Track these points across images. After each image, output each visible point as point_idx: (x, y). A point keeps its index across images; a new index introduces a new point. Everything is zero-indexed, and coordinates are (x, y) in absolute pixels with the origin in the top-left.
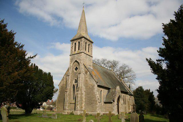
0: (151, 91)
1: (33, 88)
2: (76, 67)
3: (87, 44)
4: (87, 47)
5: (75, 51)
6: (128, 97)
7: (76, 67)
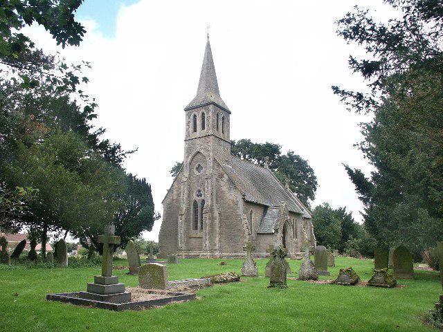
0: (176, 164)
1: (102, 204)
2: (199, 165)
3: (221, 117)
4: (220, 122)
5: (195, 130)
6: (300, 224)
7: (199, 165)
